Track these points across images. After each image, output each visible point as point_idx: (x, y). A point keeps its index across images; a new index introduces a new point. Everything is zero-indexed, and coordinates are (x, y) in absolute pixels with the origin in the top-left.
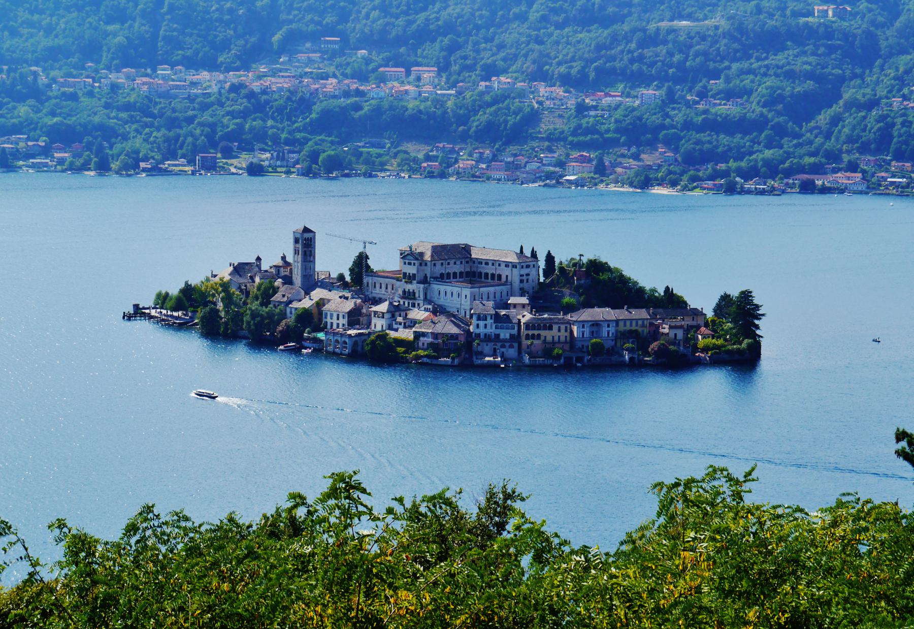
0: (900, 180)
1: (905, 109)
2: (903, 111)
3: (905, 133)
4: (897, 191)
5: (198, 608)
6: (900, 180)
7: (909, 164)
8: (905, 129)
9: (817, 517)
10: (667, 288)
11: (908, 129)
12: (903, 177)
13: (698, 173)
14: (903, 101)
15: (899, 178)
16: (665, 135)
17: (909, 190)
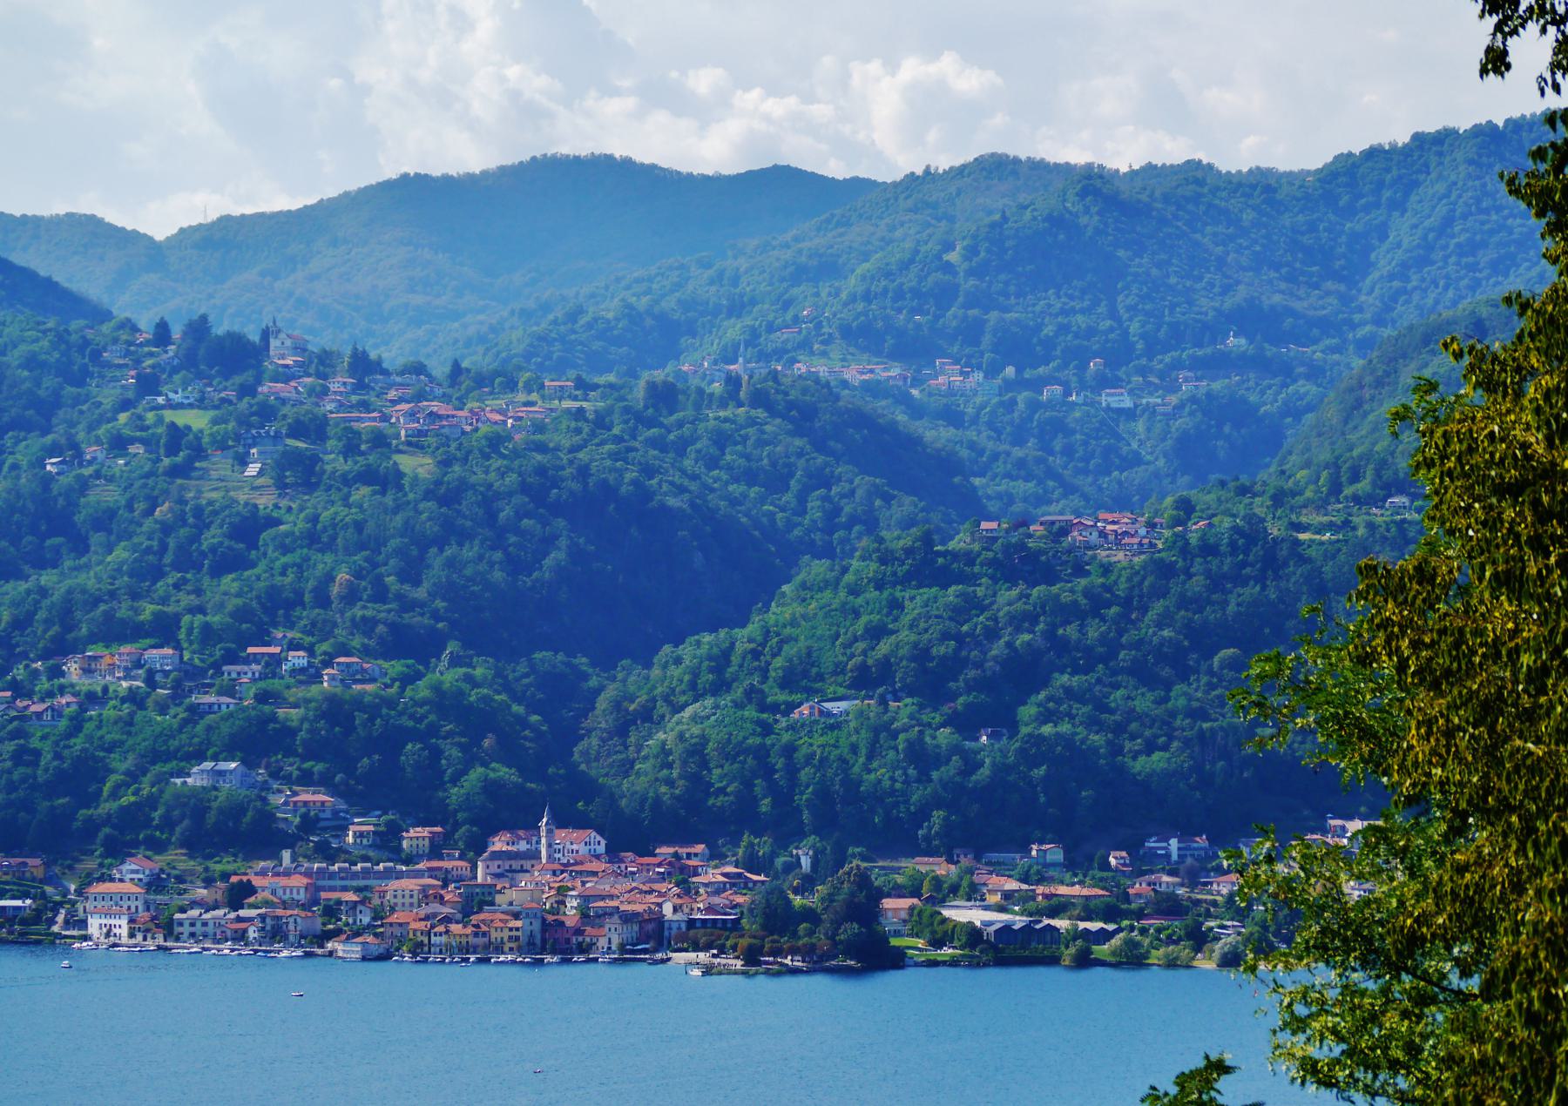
0: (18, 903)
1: (22, 718)
2: (15, 723)
3: (23, 780)
4: (11, 932)
5: (526, 675)
6: (18, 903)
7: (38, 861)
8: (22, 770)
9: (1501, 124)
10: (1482, 16)
11: (29, 771)
12: (24, 896)
13: (565, 659)
14: (14, 698)
15: (13, 898)
16: (907, 740)
17: (41, 928)
